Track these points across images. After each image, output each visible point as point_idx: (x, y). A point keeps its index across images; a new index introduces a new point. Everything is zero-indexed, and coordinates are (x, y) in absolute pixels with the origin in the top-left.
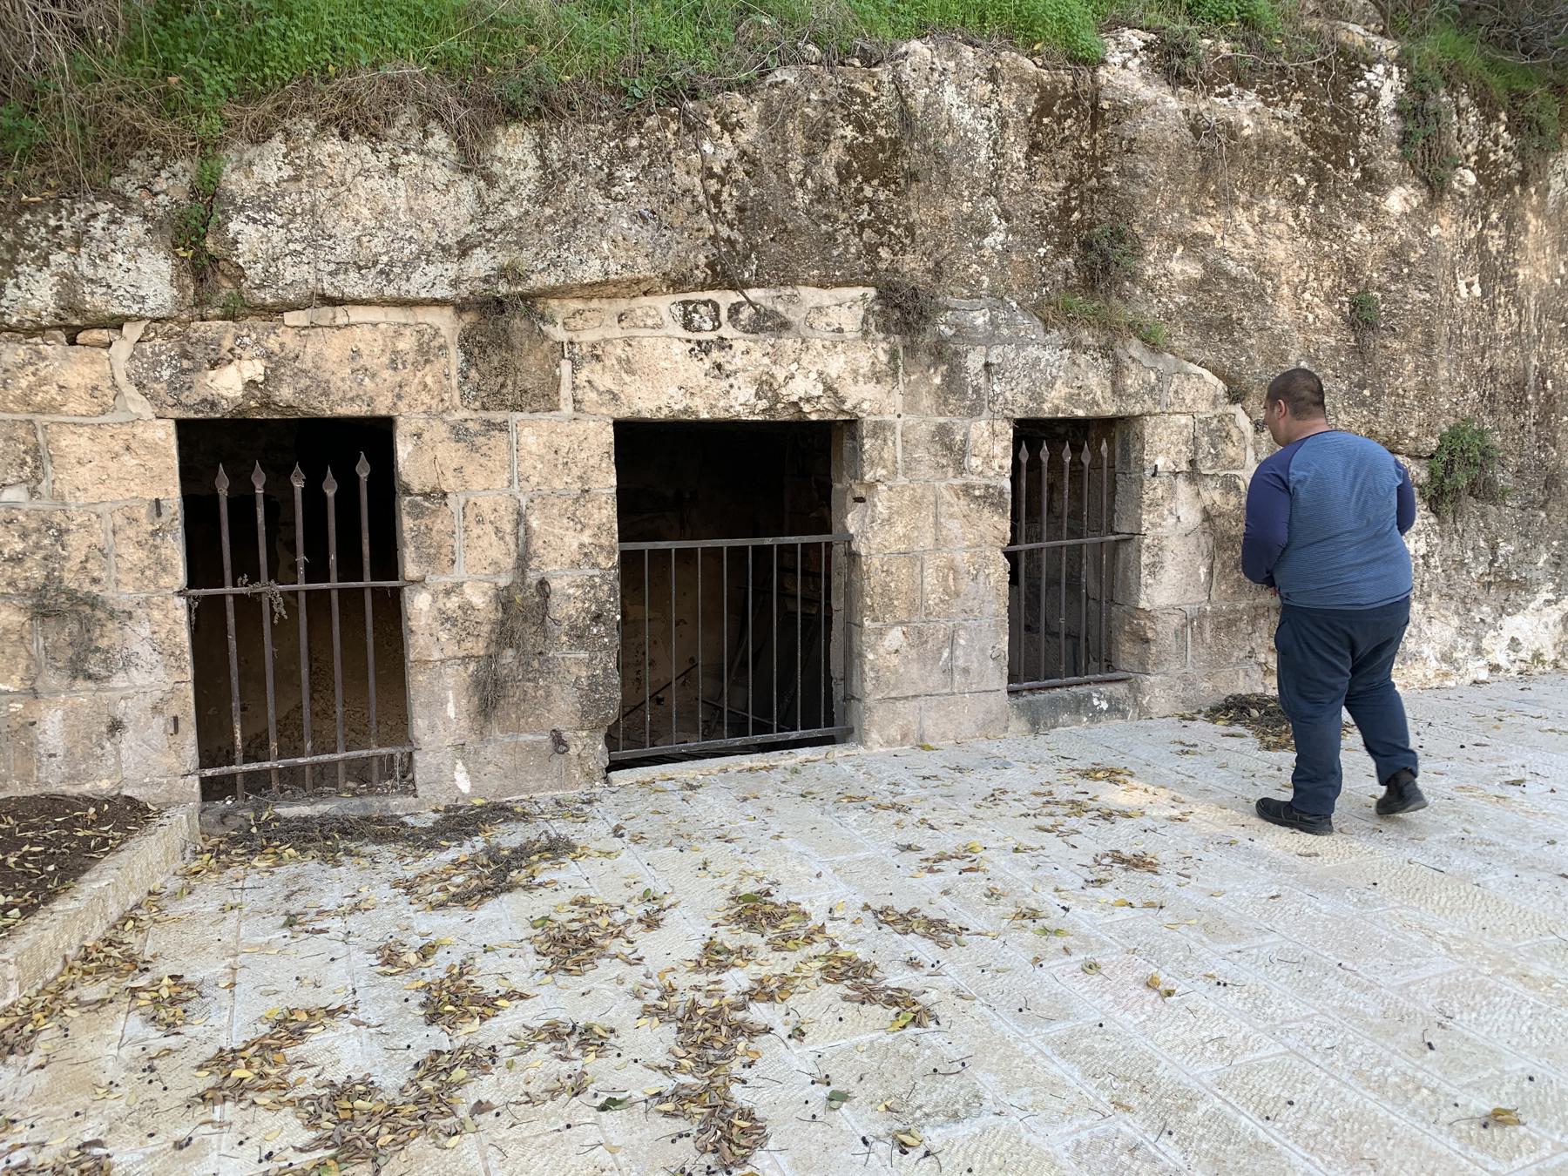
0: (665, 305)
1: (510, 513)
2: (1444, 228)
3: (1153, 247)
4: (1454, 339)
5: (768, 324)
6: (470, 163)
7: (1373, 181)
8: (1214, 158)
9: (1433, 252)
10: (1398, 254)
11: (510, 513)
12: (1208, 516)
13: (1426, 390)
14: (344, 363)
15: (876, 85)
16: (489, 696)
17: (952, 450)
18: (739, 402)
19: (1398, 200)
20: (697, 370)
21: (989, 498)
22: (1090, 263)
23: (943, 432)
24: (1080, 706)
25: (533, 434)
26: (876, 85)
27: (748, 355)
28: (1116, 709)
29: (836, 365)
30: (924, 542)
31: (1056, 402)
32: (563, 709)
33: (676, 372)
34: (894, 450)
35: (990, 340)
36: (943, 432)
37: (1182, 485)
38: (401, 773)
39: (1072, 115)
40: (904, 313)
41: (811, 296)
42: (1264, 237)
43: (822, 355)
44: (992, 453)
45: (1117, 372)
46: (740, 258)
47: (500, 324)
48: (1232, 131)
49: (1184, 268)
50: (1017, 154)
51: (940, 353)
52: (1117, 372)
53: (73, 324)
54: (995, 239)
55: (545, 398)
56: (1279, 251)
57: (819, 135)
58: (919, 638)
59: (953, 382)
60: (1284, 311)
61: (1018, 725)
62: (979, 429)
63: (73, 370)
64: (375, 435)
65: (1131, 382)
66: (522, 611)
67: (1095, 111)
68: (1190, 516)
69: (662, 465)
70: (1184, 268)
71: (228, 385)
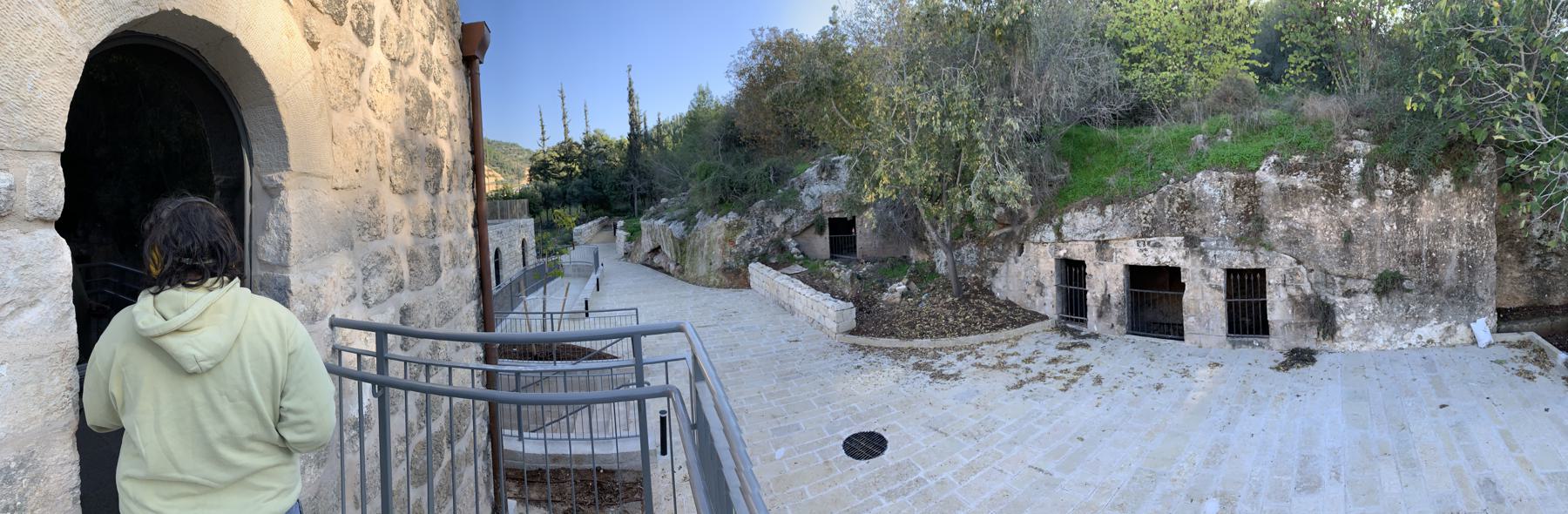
0: (1134, 241)
1: (1106, 280)
2: (1378, 210)
3: (1272, 221)
4: (1384, 244)
5: (1157, 245)
6: (1102, 213)
7: (1348, 197)
8: (1289, 196)
9: (1373, 219)
10: (1359, 219)
11: (1106, 280)
12: (1291, 296)
13: (1371, 260)
14: (1078, 251)
15: (1186, 187)
16: (1100, 315)
17: (1207, 277)
18: (1150, 262)
19: (1355, 204)
20: (1140, 255)
21: (1218, 288)
22: (1252, 227)
23: (1203, 271)
24: (1249, 343)
25: (1108, 266)
26: (1186, 187)
27: (1152, 252)
28: (1261, 345)
29: (1174, 255)
30: (1204, 300)
31: (1236, 265)
32: (1114, 320)
33: (1137, 254)
34: (1189, 275)
35: (1216, 249)
36: (1203, 271)
37: (1281, 288)
38: (1084, 322)
39: (1247, 187)
40: (1191, 242)
41: (1168, 239)
42: (1315, 218)
43: (1170, 252)
44: (1219, 278)
45: (1256, 257)
46: (1150, 231)
47: (1102, 244)
48: (1294, 188)
49: (1281, 226)
50: (1230, 198)
51: (1202, 252)
52: (1256, 257)
53: (1042, 243)
54: (1223, 221)
55: (1110, 259)
56: (1317, 220)
57: (1171, 201)
58: (1199, 320)
59: (1206, 260)
60: (1319, 237)
61: (1229, 346)
62: (1213, 271)
63: (1042, 249)
64: (1082, 264)
65: (1261, 259)
66: (1106, 299)
67: (1254, 185)
68: (1284, 296)
69: (1136, 274)
70: (1281, 226)
71: (1062, 253)
